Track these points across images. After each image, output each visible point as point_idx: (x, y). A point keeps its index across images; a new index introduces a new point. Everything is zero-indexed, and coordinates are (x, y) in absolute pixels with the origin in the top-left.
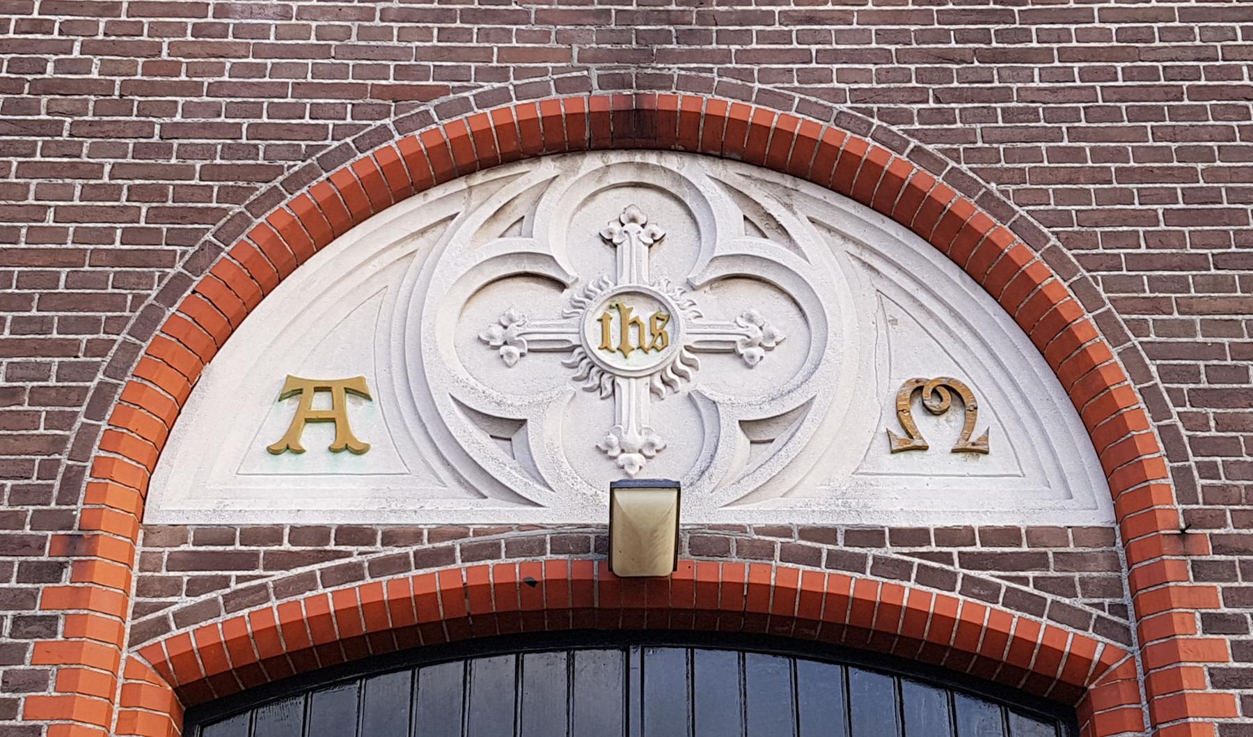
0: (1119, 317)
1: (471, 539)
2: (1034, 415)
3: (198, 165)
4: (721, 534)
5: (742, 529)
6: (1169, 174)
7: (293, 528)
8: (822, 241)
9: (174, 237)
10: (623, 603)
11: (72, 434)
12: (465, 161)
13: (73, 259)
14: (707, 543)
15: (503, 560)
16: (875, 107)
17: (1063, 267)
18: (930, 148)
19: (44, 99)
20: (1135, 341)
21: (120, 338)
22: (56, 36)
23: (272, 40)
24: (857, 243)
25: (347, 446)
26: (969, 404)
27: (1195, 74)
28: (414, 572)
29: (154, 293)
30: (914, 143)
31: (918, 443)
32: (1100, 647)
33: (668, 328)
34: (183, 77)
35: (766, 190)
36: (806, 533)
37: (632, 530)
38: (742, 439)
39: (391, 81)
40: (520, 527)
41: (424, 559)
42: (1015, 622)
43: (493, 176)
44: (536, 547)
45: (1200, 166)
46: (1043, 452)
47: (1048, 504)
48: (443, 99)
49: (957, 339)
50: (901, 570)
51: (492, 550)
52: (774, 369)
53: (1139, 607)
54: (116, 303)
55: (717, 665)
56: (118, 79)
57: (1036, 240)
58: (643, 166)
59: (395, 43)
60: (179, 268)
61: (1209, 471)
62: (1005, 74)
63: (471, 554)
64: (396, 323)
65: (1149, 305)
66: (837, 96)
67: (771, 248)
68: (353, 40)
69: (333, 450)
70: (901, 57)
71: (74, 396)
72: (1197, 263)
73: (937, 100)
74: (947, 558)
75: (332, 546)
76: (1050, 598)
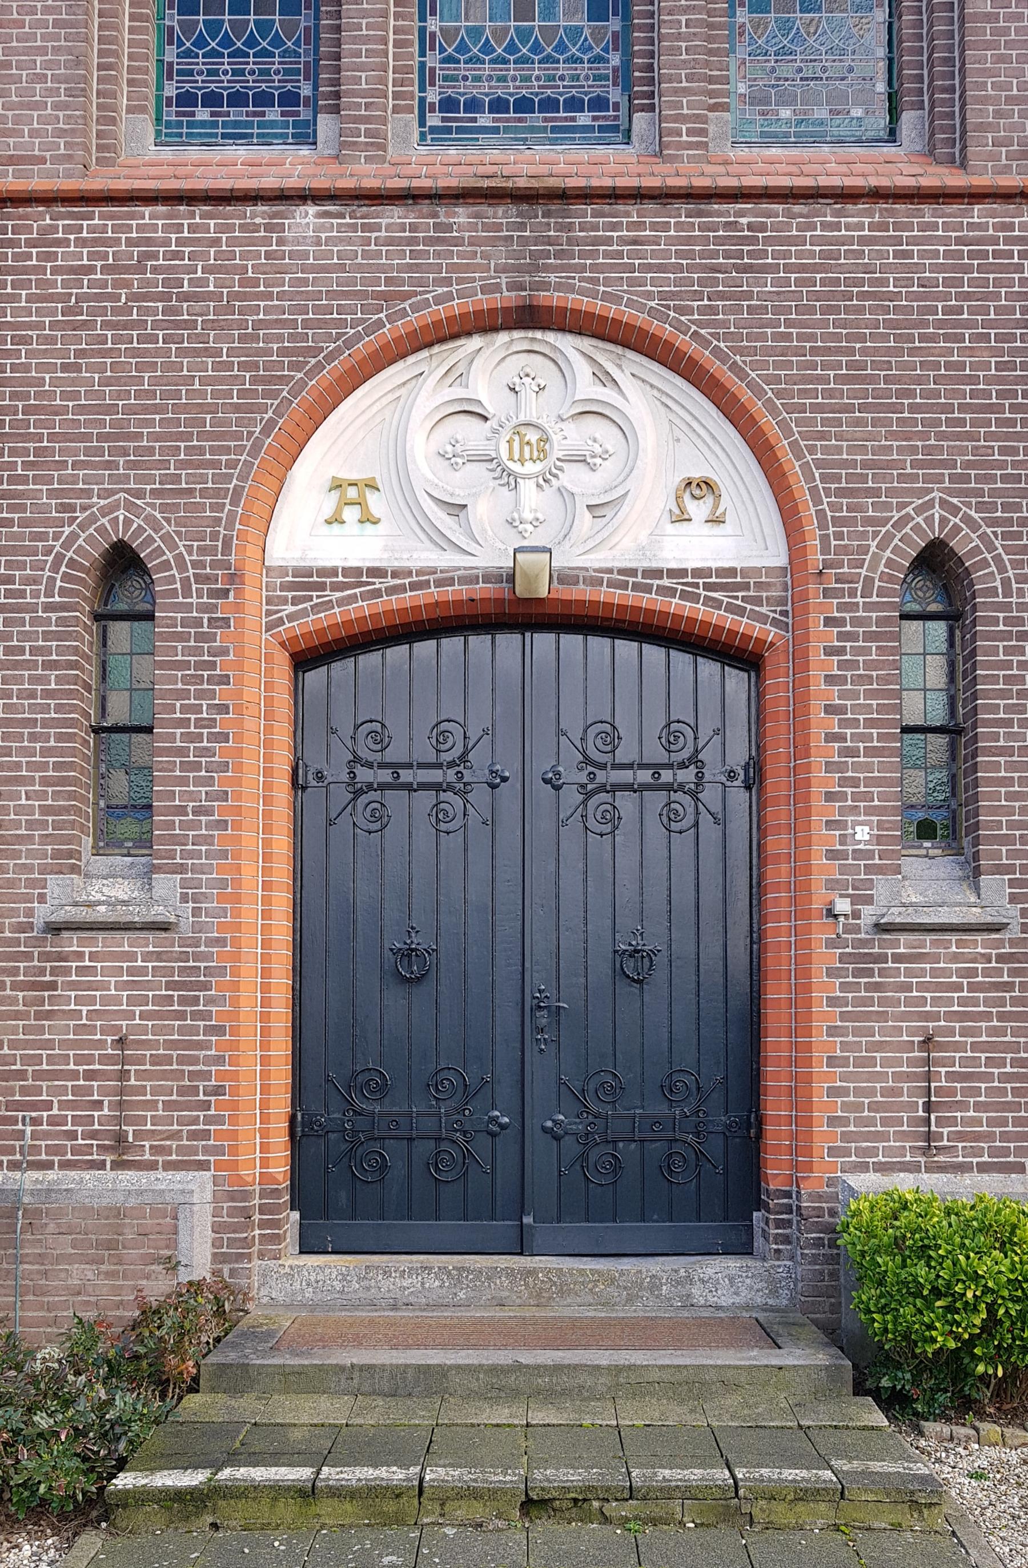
0: (802, 443)
1: (439, 575)
2: (752, 500)
3: (275, 346)
4: (575, 572)
5: (586, 569)
6: (839, 351)
7: (343, 569)
8: (640, 390)
9: (266, 394)
10: (521, 610)
11: (224, 515)
12: (428, 339)
13: (213, 409)
14: (567, 578)
15: (456, 587)
16: (672, 303)
17: (773, 410)
18: (703, 331)
19: (185, 305)
20: (809, 458)
21: (243, 458)
22: (186, 262)
23: (311, 261)
24: (659, 390)
25: (368, 519)
26: (717, 493)
27: (861, 283)
28: (409, 594)
29: (258, 430)
30: (694, 328)
31: (686, 517)
32: (772, 633)
33: (547, 447)
34: (262, 288)
35: (606, 354)
36: (622, 571)
37: (525, 574)
38: (588, 515)
39: (383, 288)
40: (465, 568)
41: (413, 586)
42: (729, 620)
43: (444, 347)
44: (473, 580)
45: (858, 345)
46: (755, 522)
47: (754, 553)
48: (414, 299)
49: (713, 452)
50: (671, 592)
51: (450, 581)
52: (608, 470)
53: (794, 613)
54: (237, 436)
55: (572, 642)
56: (225, 290)
57: (759, 393)
58: (533, 340)
59: (384, 261)
60: (270, 413)
61: (839, 536)
62: (750, 281)
63: (439, 583)
64: (392, 443)
65: (819, 435)
66: (649, 296)
67: (607, 394)
68: (359, 260)
69: (361, 522)
70: (690, 268)
71: (222, 493)
72: (848, 409)
73: (709, 299)
74: (696, 585)
75: (364, 579)
76: (749, 607)
